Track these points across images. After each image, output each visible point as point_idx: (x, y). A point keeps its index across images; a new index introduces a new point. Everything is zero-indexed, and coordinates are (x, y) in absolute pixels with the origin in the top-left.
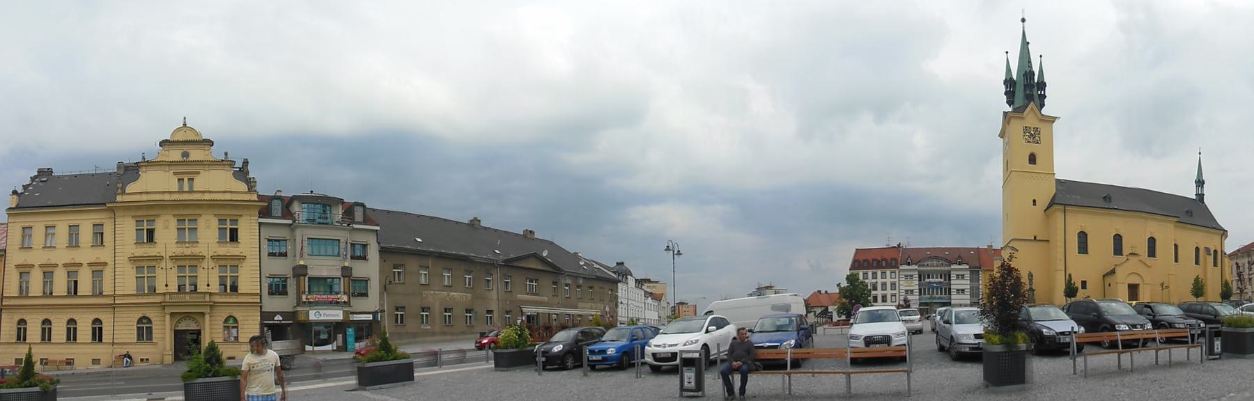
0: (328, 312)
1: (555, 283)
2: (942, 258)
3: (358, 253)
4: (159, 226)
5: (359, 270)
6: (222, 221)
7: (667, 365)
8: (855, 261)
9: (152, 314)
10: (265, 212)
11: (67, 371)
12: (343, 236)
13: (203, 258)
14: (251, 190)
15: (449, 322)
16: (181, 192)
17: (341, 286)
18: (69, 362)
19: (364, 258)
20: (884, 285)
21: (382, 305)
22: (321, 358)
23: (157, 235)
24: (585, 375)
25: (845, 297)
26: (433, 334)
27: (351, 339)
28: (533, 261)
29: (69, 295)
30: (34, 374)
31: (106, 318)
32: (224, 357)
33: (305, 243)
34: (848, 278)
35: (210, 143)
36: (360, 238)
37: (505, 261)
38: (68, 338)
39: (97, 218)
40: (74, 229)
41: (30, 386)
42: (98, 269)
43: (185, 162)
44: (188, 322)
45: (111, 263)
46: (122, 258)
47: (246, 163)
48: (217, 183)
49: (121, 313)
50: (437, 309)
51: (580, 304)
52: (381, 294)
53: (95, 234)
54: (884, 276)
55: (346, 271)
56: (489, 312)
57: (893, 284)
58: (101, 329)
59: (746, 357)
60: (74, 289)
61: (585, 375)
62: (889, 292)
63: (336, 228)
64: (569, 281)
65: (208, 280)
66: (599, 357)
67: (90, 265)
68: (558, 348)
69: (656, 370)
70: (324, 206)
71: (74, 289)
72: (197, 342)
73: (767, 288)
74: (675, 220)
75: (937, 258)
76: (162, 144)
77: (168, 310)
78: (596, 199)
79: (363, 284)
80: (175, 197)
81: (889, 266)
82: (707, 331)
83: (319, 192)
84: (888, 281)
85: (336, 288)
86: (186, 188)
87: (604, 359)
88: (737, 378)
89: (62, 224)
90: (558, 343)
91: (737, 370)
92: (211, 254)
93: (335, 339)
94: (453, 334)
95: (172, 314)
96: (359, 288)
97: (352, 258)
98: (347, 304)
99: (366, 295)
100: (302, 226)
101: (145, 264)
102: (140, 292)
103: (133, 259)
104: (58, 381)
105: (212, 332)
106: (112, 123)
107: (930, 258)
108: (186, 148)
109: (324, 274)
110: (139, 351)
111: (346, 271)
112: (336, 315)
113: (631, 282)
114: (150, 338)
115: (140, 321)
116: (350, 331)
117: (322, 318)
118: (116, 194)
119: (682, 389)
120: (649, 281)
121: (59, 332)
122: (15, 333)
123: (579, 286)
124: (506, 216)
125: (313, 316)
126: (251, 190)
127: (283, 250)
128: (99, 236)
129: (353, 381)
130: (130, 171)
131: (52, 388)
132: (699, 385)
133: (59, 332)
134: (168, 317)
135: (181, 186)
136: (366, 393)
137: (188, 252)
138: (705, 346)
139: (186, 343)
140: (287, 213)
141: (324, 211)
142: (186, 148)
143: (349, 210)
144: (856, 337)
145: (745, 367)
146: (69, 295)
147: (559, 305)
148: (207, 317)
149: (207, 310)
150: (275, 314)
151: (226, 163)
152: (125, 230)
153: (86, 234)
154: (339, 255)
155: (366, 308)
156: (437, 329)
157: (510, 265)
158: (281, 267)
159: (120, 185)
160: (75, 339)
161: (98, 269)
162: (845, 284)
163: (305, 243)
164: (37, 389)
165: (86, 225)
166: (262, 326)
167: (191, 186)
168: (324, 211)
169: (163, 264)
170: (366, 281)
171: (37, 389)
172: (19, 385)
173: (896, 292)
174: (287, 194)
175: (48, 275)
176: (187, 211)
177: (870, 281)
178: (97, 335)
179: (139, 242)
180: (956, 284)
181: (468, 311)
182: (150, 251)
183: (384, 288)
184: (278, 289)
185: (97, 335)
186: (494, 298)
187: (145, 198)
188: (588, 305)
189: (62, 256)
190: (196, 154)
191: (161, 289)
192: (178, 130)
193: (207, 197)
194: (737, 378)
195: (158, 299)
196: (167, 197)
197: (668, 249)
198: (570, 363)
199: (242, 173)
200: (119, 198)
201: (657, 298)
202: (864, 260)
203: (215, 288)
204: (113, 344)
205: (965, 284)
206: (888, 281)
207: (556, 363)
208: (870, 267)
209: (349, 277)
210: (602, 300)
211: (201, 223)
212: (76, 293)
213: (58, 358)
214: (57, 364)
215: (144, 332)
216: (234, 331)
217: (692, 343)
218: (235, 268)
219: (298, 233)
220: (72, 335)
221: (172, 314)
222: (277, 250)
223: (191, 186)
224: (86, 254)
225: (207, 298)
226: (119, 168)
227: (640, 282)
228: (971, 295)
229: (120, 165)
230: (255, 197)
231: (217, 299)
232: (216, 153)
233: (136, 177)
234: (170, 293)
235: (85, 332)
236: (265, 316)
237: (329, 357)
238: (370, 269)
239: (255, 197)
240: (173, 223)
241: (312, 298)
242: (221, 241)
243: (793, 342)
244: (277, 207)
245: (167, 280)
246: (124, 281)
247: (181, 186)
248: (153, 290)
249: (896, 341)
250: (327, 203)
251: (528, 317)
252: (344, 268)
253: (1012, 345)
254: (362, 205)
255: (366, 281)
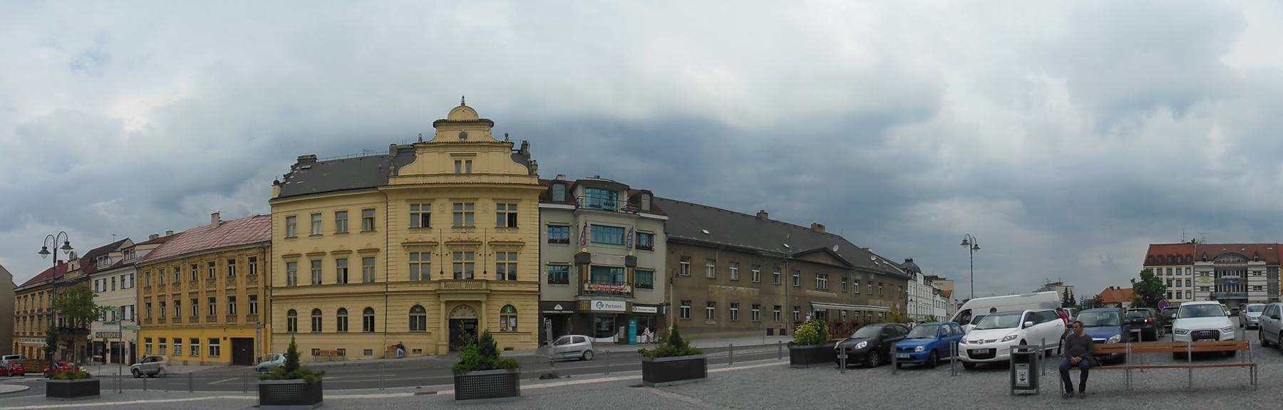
0: (610, 303)
1: (845, 279)
2: (1238, 255)
3: (644, 243)
4: (435, 210)
5: (645, 260)
6: (501, 206)
7: (984, 362)
8: (1149, 256)
9: (426, 303)
10: (546, 197)
11: (339, 362)
12: (628, 224)
13: (480, 243)
14: (532, 173)
15: (742, 318)
16: (458, 174)
17: (624, 276)
18: (341, 353)
19: (650, 248)
20: (1179, 281)
21: (667, 297)
22: (603, 350)
23: (433, 220)
24: (894, 373)
25: (1140, 293)
26: (718, 329)
27: (633, 331)
28: (821, 256)
29: (339, 283)
30: (297, 366)
31: (378, 307)
32: (500, 347)
33: (589, 230)
34: (1142, 274)
35: (490, 123)
36: (646, 227)
37: (794, 256)
38: (339, 328)
39: (367, 202)
40: (341, 216)
41: (295, 378)
42: (368, 256)
43: (463, 143)
44: (464, 310)
45: (383, 249)
46: (395, 244)
47: (525, 145)
48: (496, 165)
49: (393, 302)
50: (723, 303)
51: (871, 301)
52: (667, 287)
53: (364, 219)
54: (1179, 272)
55: (631, 261)
56: (777, 307)
57: (1188, 281)
58: (372, 318)
59: (1080, 355)
60: (344, 277)
61: (894, 373)
62: (1184, 288)
63: (621, 216)
64: (859, 277)
65: (486, 267)
66: (907, 355)
67: (360, 251)
68: (862, 345)
69: (969, 367)
70: (611, 192)
71: (344, 277)
72: (473, 332)
73: (1056, 284)
74: (962, 216)
75: (1233, 254)
76: (436, 124)
77: (443, 299)
78: (885, 194)
79: (648, 276)
80: (453, 179)
81: (1184, 262)
82: (1024, 327)
83: (605, 177)
84: (1183, 277)
85: (619, 278)
86: (464, 171)
87: (913, 358)
88: (1075, 377)
89: (328, 211)
90: (861, 339)
91: (1076, 365)
92: (489, 239)
93: (617, 331)
94: (739, 330)
95: (447, 303)
96: (644, 280)
97: (637, 247)
98: (630, 295)
99: (651, 287)
100: (584, 212)
101: (420, 250)
102: (413, 280)
103: (407, 245)
104: (323, 373)
105: (489, 321)
106: (383, 102)
107: (1227, 254)
108: (464, 129)
109: (608, 263)
110: (413, 341)
111: (631, 261)
112: (619, 306)
113: (920, 280)
114: (423, 327)
115: (413, 310)
116: (633, 323)
117: (604, 309)
118: (388, 177)
119: (1014, 386)
120: (936, 278)
121: (329, 322)
122: (286, 323)
123: (870, 282)
124: (793, 210)
125: (595, 306)
126: (532, 173)
127: (565, 237)
128: (369, 223)
129: (638, 376)
130: (405, 153)
131: (316, 379)
132: (1033, 383)
133: (329, 322)
134: (443, 306)
135: (458, 169)
136: (653, 390)
137: (464, 237)
138: (1023, 342)
139: (462, 332)
140: (570, 197)
141: (611, 198)
142: (464, 128)
143: (635, 198)
144: (1183, 332)
145: (1085, 363)
146: (339, 283)
147: (848, 302)
148: (484, 305)
149: (483, 299)
150: (556, 303)
151: (506, 144)
152: (399, 215)
153: (355, 220)
154: (623, 244)
155: (650, 300)
156: (723, 324)
157: (798, 259)
158: (562, 254)
159: (392, 168)
160: (346, 328)
161: (368, 256)
162: (1139, 280)
163: (589, 230)
164: (301, 381)
165: (355, 209)
166: (541, 316)
167: (469, 168)
168: (611, 198)
169: (438, 251)
170: (651, 272)
171: (301, 381)
172: (284, 376)
173: (1191, 288)
174: (571, 178)
175: (316, 264)
176: (463, 195)
177: (1164, 278)
178: (369, 324)
179: (413, 228)
180: (1253, 280)
181: (755, 306)
182: (426, 236)
183: (671, 281)
184: (559, 278)
185: (369, 324)
186: (782, 294)
187: (421, 180)
188: (878, 302)
189: (330, 243)
190: (474, 135)
191: (435, 276)
192: (456, 109)
193: (485, 179)
194: (1075, 377)
195: (432, 287)
196: (442, 180)
197: (965, 243)
198: (874, 360)
199: (522, 155)
200: (391, 181)
201: (946, 295)
202: (1158, 256)
203: (492, 276)
204: (386, 333)
205: (1262, 280)
206: (1183, 277)
207: (860, 360)
208: (1165, 263)
209: (634, 266)
210: (891, 298)
211: (478, 208)
212: (346, 281)
213: (329, 348)
214: (329, 355)
215: (418, 321)
216: (512, 321)
217: (1011, 338)
218: (514, 255)
219: (581, 220)
220: (342, 325)
221: (447, 303)
222: (558, 237)
223: (469, 168)
224: (356, 241)
225: (484, 286)
226: (391, 150)
227: (929, 279)
228: (1269, 292)
229: (393, 147)
230: (535, 181)
231: (494, 287)
232: (496, 134)
233: (413, 159)
234: (445, 281)
235: (356, 322)
236: (543, 305)
237: (612, 349)
238: (656, 260)
239: (535, 181)
240: (449, 207)
241: (594, 287)
242: (500, 226)
243: (1118, 337)
244: (559, 192)
245: (442, 266)
246: (397, 268)
247: (458, 169)
248: (427, 278)
249: (1225, 336)
250: (613, 188)
251: (817, 313)
252: (628, 258)
253: (477, 363)
254: (649, 193)
255: (651, 272)
